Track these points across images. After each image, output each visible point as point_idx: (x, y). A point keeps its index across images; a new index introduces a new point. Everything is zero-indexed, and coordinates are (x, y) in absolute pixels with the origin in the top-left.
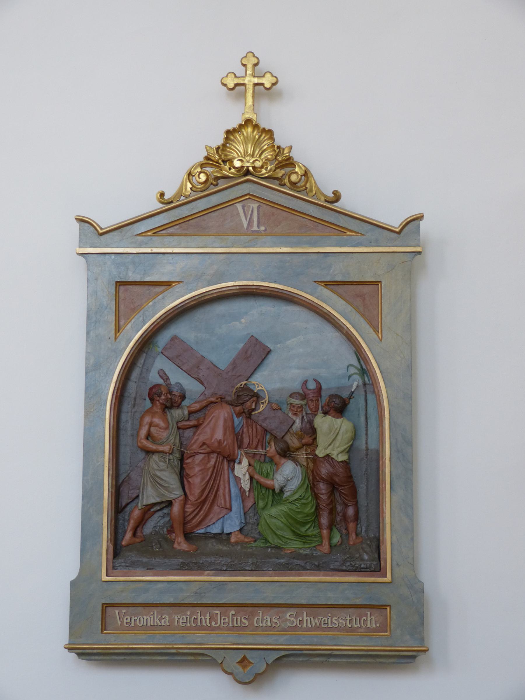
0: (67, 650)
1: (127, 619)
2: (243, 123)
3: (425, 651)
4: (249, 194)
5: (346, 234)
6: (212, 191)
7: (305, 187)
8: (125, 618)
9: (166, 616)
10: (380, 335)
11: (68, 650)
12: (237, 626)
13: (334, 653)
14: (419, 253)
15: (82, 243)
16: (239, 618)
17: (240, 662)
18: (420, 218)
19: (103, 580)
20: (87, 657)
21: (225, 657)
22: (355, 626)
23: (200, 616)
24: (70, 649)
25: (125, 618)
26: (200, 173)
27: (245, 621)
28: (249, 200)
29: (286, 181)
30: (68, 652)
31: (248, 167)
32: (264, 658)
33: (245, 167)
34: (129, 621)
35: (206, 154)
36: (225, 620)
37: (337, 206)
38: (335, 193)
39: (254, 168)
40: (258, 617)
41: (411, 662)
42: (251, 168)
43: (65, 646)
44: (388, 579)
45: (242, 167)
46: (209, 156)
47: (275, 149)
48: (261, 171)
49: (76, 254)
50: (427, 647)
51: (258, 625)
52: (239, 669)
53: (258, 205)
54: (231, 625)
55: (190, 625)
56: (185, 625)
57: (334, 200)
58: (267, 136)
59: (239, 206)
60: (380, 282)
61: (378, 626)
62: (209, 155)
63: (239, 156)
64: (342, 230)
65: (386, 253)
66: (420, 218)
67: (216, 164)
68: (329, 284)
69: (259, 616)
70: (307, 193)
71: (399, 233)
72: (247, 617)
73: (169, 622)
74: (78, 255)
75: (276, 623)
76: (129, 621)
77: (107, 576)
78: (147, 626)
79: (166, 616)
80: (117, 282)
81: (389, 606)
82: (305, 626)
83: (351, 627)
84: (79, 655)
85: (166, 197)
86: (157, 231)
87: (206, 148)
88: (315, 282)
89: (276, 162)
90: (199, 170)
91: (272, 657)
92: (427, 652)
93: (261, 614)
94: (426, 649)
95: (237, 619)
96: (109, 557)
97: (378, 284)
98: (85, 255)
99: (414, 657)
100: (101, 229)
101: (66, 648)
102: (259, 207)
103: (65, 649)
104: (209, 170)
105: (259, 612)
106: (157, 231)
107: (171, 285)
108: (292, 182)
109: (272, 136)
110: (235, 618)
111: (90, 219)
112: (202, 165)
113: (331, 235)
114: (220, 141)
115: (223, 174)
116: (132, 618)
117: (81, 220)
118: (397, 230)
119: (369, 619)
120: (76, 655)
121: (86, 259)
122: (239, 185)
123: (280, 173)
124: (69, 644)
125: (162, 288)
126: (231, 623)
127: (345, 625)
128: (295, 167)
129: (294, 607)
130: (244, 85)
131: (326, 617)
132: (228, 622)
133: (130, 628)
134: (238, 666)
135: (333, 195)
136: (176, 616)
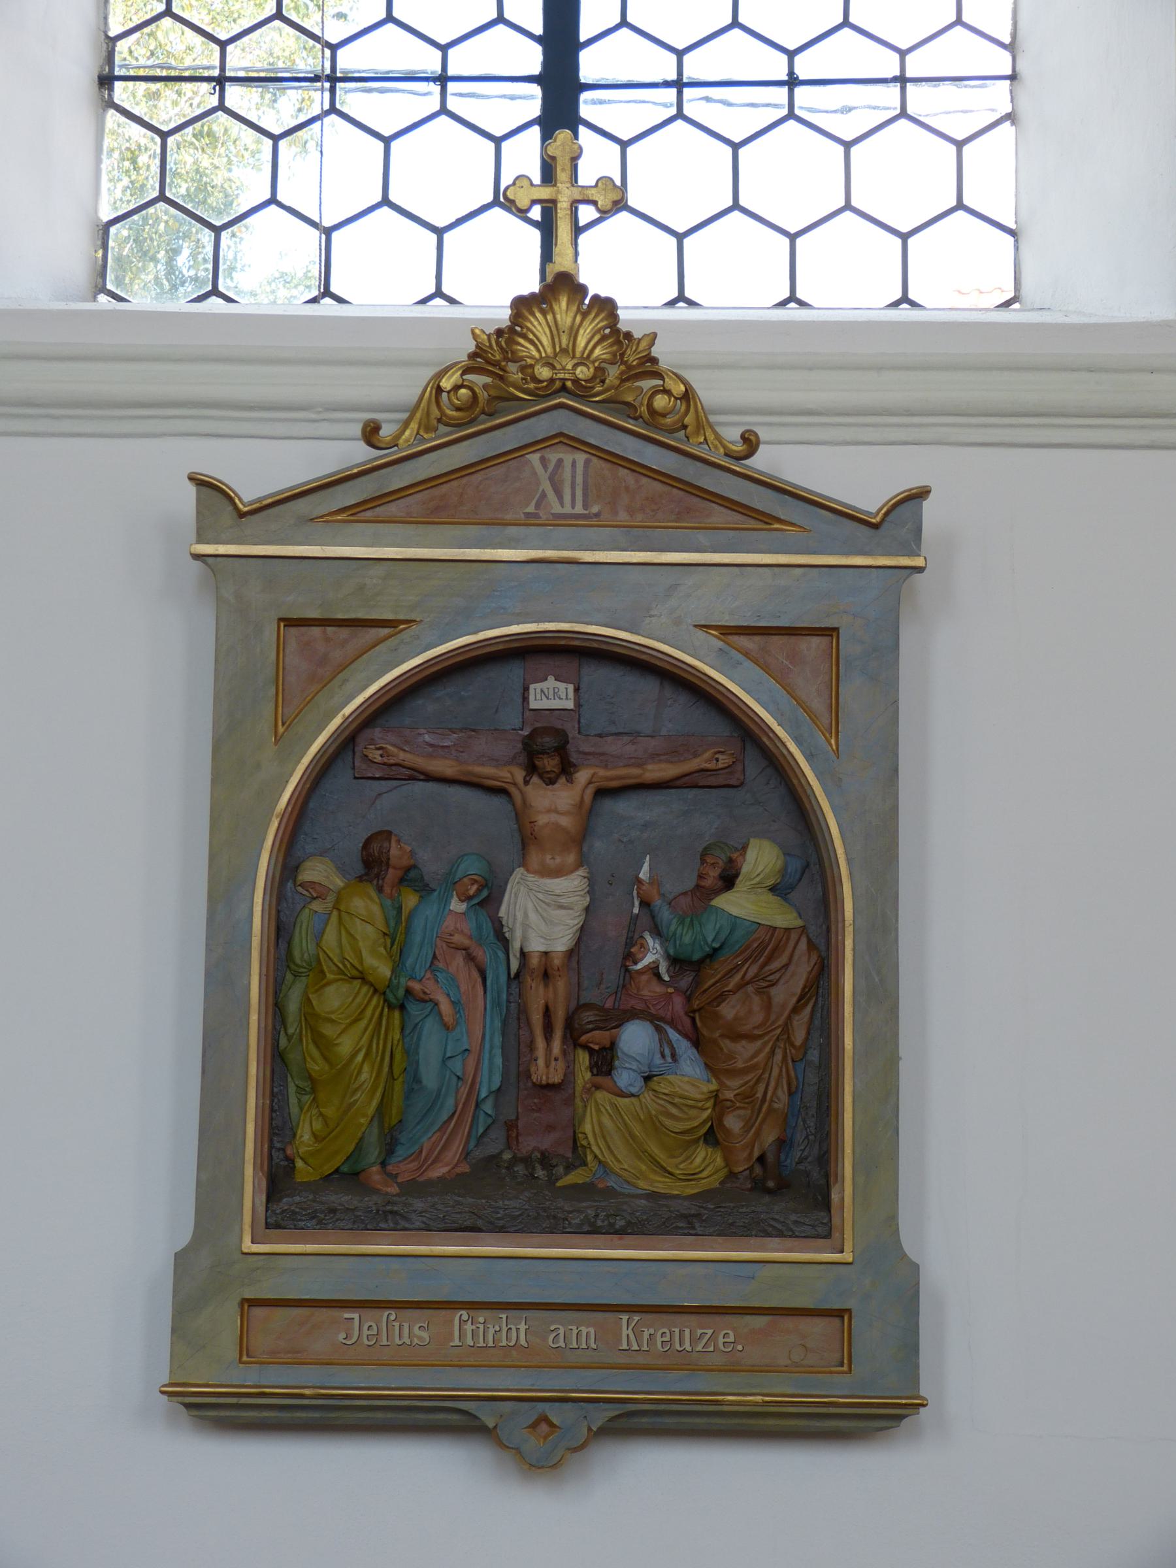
4: (561, 434)
6: (482, 427)
8: (366, 1327)
10: (833, 742)
12: (400, 1343)
14: (920, 570)
16: (677, 1330)
17: (534, 1426)
18: (920, 494)
19: (245, 1251)
24: (170, 1394)
25: (366, 1327)
28: (560, 445)
33: (557, 382)
34: (667, 1339)
37: (760, 462)
39: (576, 381)
41: (892, 1427)
42: (569, 384)
44: (847, 1256)
45: (552, 381)
48: (593, 388)
49: (190, 557)
51: (682, 1349)
57: (742, 454)
59: (535, 458)
66: (920, 494)
68: (727, 631)
70: (687, 437)
71: (242, 515)
72: (426, 1326)
75: (420, 1338)
76: (667, 1339)
77: (253, 1242)
78: (640, 1350)
79: (560, 1327)
84: (188, 1406)
88: (695, 626)
91: (601, 1416)
92: (922, 1410)
94: (925, 1402)
96: (257, 1201)
97: (831, 636)
99: (900, 1418)
101: (163, 1393)
102: (587, 462)
106: (356, 512)
108: (653, 408)
110: (397, 1324)
111: (210, 477)
112: (467, 370)
117: (202, 483)
119: (505, 1329)
120: (182, 1407)
125: (385, 632)
127: (354, 1340)
129: (720, 1313)
135: (739, 448)
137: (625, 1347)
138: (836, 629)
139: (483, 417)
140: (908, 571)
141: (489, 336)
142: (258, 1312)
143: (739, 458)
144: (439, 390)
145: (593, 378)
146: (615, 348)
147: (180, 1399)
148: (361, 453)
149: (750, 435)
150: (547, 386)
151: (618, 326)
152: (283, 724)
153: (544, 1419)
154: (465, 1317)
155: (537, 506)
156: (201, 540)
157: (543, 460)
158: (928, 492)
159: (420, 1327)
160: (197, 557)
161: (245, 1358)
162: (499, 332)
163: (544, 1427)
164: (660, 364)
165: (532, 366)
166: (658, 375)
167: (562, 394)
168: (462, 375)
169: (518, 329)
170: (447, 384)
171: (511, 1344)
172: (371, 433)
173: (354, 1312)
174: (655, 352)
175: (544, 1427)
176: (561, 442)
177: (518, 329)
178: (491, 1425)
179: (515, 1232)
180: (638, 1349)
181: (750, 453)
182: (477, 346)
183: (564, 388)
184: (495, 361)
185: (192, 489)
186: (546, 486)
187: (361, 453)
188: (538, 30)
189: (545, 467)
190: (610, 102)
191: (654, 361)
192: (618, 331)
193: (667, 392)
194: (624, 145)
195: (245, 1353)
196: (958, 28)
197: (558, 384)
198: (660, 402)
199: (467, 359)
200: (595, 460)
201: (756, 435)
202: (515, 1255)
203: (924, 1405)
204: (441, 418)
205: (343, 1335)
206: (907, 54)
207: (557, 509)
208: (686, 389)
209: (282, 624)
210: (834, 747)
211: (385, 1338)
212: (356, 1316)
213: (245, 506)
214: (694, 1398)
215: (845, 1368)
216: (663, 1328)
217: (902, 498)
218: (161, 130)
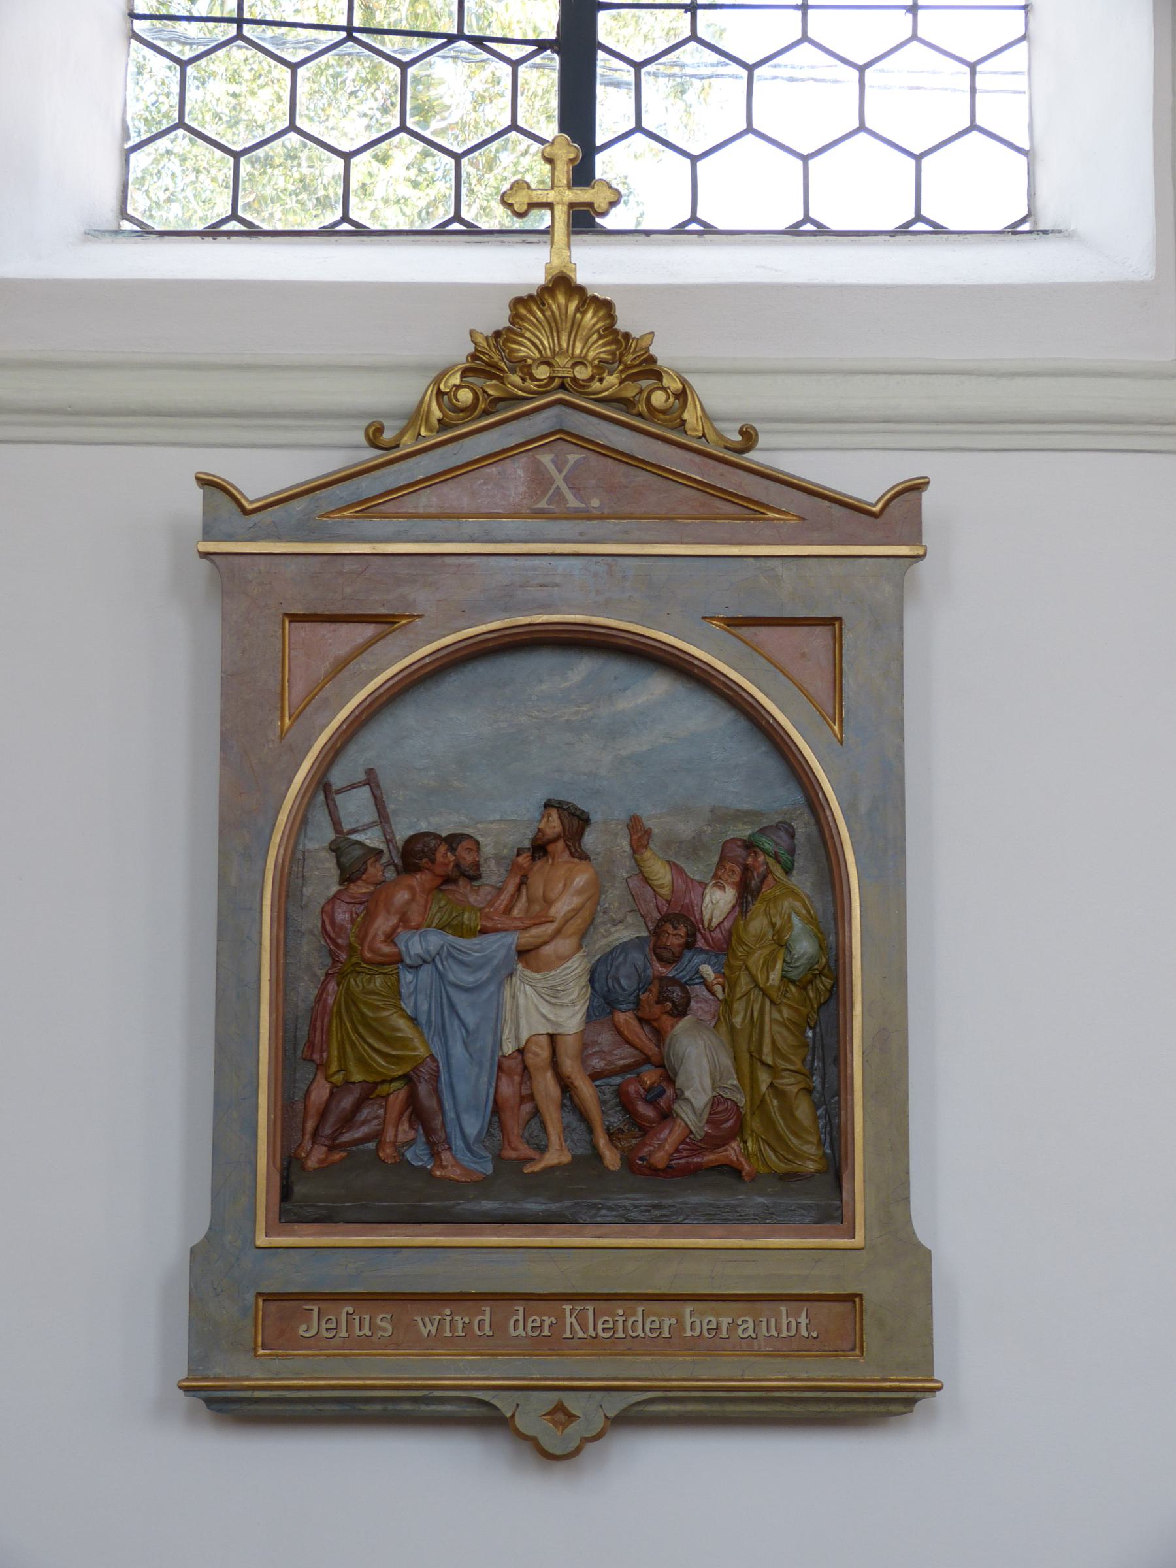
0: (181, 1392)
2: (551, 285)
3: (933, 1390)
9: (747, 1319)
10: (836, 728)
13: (431, 1395)
15: (207, 535)
16: (367, 1317)
18: (916, 487)
21: (518, 1405)
22: (513, 1334)
23: (787, 1318)
24: (186, 1389)
25: (531, 1319)
26: (458, 387)
27: (385, 1325)
28: (560, 441)
29: (642, 407)
30: (186, 1396)
33: (557, 379)
35: (471, 349)
37: (755, 457)
38: (741, 432)
39: (574, 379)
40: (515, 1318)
44: (859, 1240)
45: (551, 379)
47: (620, 338)
48: (589, 386)
49: (197, 554)
50: (937, 1382)
54: (620, 1335)
55: (624, 1336)
56: (611, 1333)
57: (738, 446)
60: (839, 619)
64: (752, 508)
65: (846, 559)
66: (916, 487)
68: (733, 623)
69: (518, 1315)
72: (389, 1317)
73: (370, 1330)
74: (201, 558)
76: (538, 1324)
80: (286, 615)
81: (860, 1296)
82: (620, 1335)
83: (596, 1337)
84: (209, 1402)
87: (650, 333)
89: (621, 367)
90: (456, 380)
91: (616, 1404)
93: (521, 1313)
99: (911, 1402)
100: (875, 505)
101: (181, 1388)
105: (517, 1308)
106: (367, 507)
107: (397, 623)
112: (465, 372)
114: (502, 321)
115: (509, 392)
116: (544, 1320)
117: (207, 483)
121: (212, 561)
123: (630, 391)
124: (187, 1379)
129: (590, 1300)
130: (550, 206)
131: (540, 1317)
132: (614, 1329)
133: (439, 1341)
135: (739, 438)
137: (568, 1335)
138: (839, 619)
141: (487, 338)
143: (740, 451)
144: (440, 393)
145: (592, 378)
146: (613, 347)
147: (203, 1394)
148: (369, 455)
150: (545, 384)
151: (616, 327)
153: (560, 1408)
156: (207, 535)
158: (928, 483)
160: (205, 555)
162: (497, 334)
164: (659, 363)
165: (530, 366)
166: (658, 375)
168: (462, 377)
173: (314, 1305)
175: (561, 1417)
176: (561, 439)
178: (508, 1415)
180: (451, 1335)
182: (476, 350)
183: (562, 387)
185: (198, 493)
187: (369, 455)
188: (601, 54)
191: (652, 360)
192: (617, 332)
193: (664, 389)
194: (694, 160)
196: (915, 43)
197: (557, 382)
198: (658, 399)
199: (464, 360)
201: (754, 429)
202: (685, 1246)
203: (939, 1389)
204: (443, 419)
205: (304, 1327)
206: (858, 65)
208: (684, 388)
211: (344, 1328)
215: (857, 1352)
218: (232, 150)
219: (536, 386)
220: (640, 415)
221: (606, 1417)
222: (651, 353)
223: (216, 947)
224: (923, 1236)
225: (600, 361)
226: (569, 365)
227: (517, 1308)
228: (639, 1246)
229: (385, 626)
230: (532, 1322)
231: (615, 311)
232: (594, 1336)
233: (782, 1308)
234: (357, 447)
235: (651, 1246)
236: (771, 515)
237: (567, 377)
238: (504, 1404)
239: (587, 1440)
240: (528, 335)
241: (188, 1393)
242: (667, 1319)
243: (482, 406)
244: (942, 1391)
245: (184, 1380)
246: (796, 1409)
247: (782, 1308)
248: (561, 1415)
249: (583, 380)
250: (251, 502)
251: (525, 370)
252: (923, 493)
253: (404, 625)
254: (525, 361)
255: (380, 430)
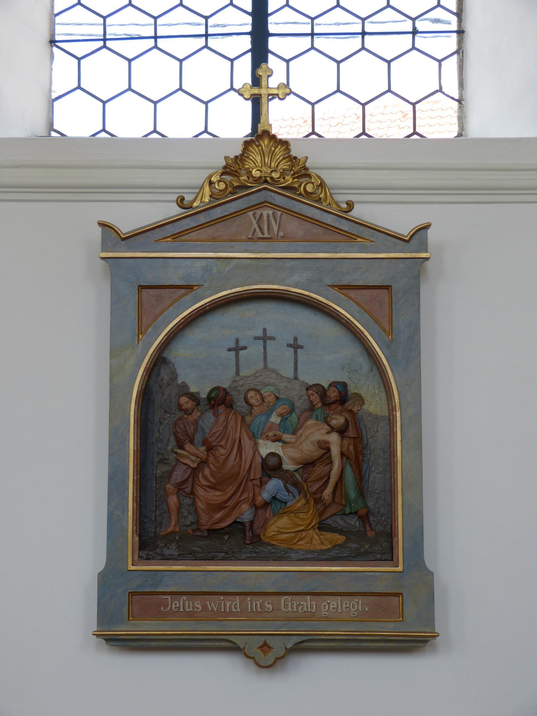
1: (175, 604)
3: (435, 637)
5: (356, 240)
7: (319, 197)
8: (174, 604)
11: (97, 636)
14: (427, 259)
17: (261, 647)
18: (427, 227)
20: (118, 644)
21: (246, 643)
22: (188, 610)
23: (310, 603)
24: (98, 636)
27: (268, 606)
30: (97, 638)
31: (265, 177)
32: (284, 644)
33: (263, 177)
35: (224, 164)
36: (347, 605)
39: (272, 178)
40: (236, 603)
42: (268, 179)
43: (93, 633)
44: (400, 569)
45: (260, 177)
46: (227, 166)
49: (99, 258)
52: (259, 654)
53: (273, 211)
54: (182, 610)
56: (177, 610)
58: (283, 147)
60: (390, 286)
61: (367, 610)
62: (228, 165)
63: (256, 166)
66: (427, 227)
67: (235, 174)
68: (341, 287)
69: (237, 602)
76: (178, 606)
77: (398, 567)
80: (139, 286)
82: (182, 610)
84: (106, 640)
85: (185, 202)
86: (176, 236)
89: (292, 173)
90: (218, 178)
92: (437, 638)
93: (238, 600)
95: (189, 603)
98: (106, 259)
99: (426, 642)
102: (281, 215)
103: (92, 635)
104: (228, 178)
105: (338, 598)
106: (176, 236)
107: (192, 288)
109: (289, 147)
113: (247, 212)
114: (238, 151)
117: (102, 224)
118: (407, 239)
120: (104, 640)
121: (106, 261)
122: (395, 239)
124: (97, 631)
126: (182, 608)
128: (311, 178)
132: (179, 607)
134: (259, 651)
136: (254, 602)
139: (230, 195)
140: (424, 260)
142: (136, 598)
145: (280, 177)
146: (289, 163)
148: (175, 211)
149: (350, 202)
152: (141, 334)
153: (265, 644)
154: (185, 598)
155: (253, 235)
156: (103, 250)
157: (254, 215)
158: (430, 225)
159: (268, 603)
161: (131, 618)
163: (265, 648)
166: (309, 176)
167: (265, 183)
168: (221, 176)
169: (246, 155)
170: (213, 179)
171: (313, 611)
172: (181, 202)
174: (307, 165)
177: (246, 155)
178: (242, 648)
179: (246, 559)
181: (350, 211)
182: (227, 164)
183: (266, 181)
184: (235, 170)
185: (99, 229)
186: (255, 226)
187: (175, 211)
189: (255, 218)
190: (438, 36)
195: (131, 615)
198: (310, 188)
200: (284, 214)
203: (438, 636)
207: (260, 235)
209: (140, 288)
210: (391, 340)
212: (169, 597)
213: (124, 236)
214: (371, 633)
215: (401, 619)
216: (176, 601)
217: (422, 227)
219: (254, 181)
220: (300, 194)
221: (286, 648)
222: (306, 166)
223: (422, 429)
224: (430, 565)
225: (283, 170)
226: (269, 172)
227: (338, 598)
228: (230, 570)
229: (189, 290)
230: (175, 605)
231: (51, 134)
232: (192, 611)
233: (308, 598)
234: (359, 202)
235: (377, 571)
236: (359, 240)
237: (268, 177)
238: (239, 641)
239: (277, 659)
240: (251, 157)
241: (98, 637)
242: (228, 602)
243: (230, 189)
244: (439, 636)
245: (94, 632)
246: (217, 644)
247: (308, 598)
248: (265, 647)
249: (277, 178)
250: (124, 234)
251: (249, 173)
252: (428, 230)
253: (196, 289)
254: (249, 169)
255: (183, 199)
